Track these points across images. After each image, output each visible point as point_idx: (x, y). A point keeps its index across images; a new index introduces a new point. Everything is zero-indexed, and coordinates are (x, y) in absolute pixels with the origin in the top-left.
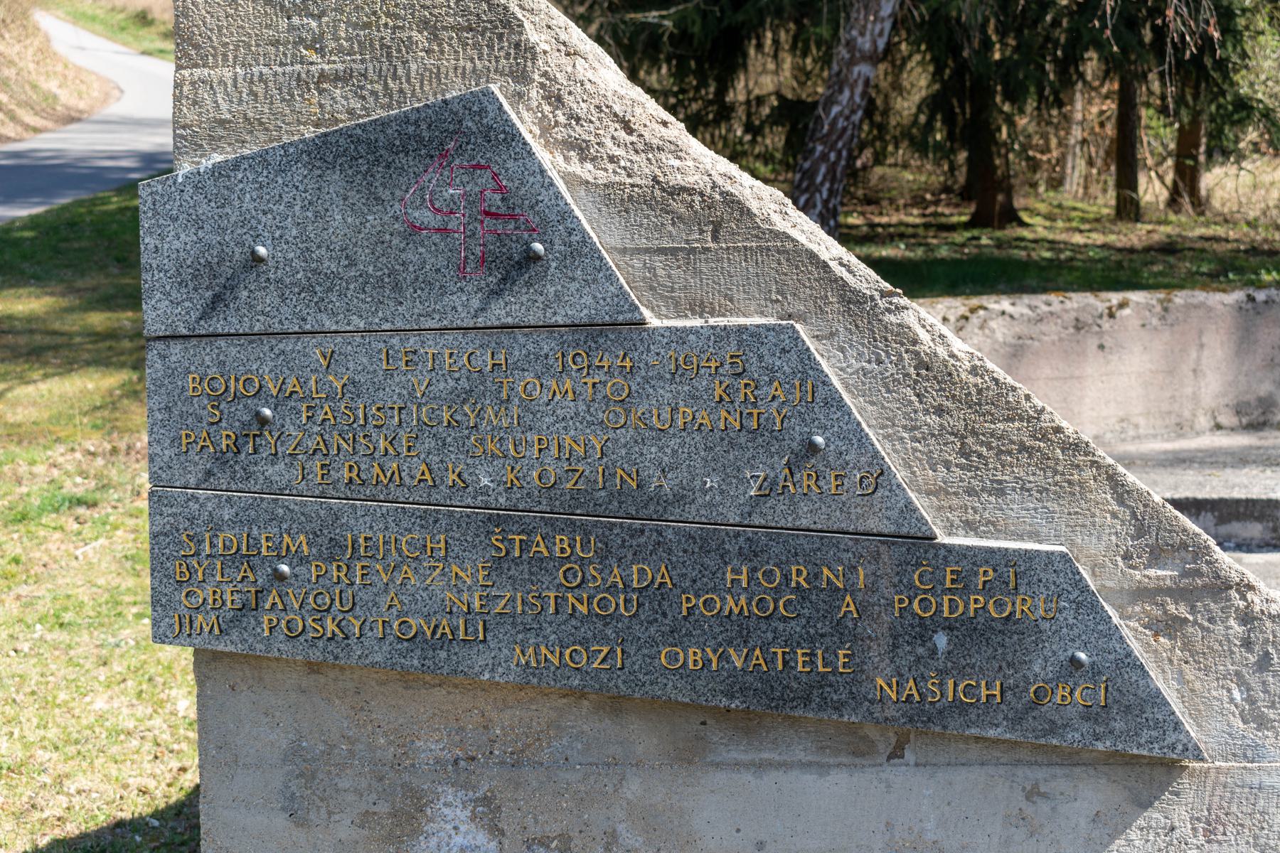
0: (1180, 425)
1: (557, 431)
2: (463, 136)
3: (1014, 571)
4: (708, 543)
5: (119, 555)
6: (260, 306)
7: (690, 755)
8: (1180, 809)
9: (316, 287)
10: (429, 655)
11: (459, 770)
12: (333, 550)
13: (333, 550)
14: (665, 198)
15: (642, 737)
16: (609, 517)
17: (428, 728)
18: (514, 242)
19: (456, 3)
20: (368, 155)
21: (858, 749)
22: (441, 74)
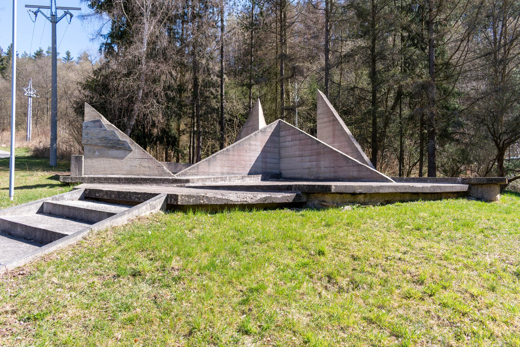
0: (55, 335)
1: (103, 134)
2: (99, 121)
3: (124, 141)
4: (110, 140)
5: (264, 62)
6: (88, 128)
7: (109, 150)
8: (132, 153)
9: (91, 127)
10: (96, 145)
11: (97, 150)
12: (92, 139)
13: (92, 139)
14: (108, 125)
15: (106, 149)
16: (105, 138)
17: (96, 148)
18: (101, 126)
19: (519, 93)
20: (94, 122)
21: (117, 149)
22: (98, 118)
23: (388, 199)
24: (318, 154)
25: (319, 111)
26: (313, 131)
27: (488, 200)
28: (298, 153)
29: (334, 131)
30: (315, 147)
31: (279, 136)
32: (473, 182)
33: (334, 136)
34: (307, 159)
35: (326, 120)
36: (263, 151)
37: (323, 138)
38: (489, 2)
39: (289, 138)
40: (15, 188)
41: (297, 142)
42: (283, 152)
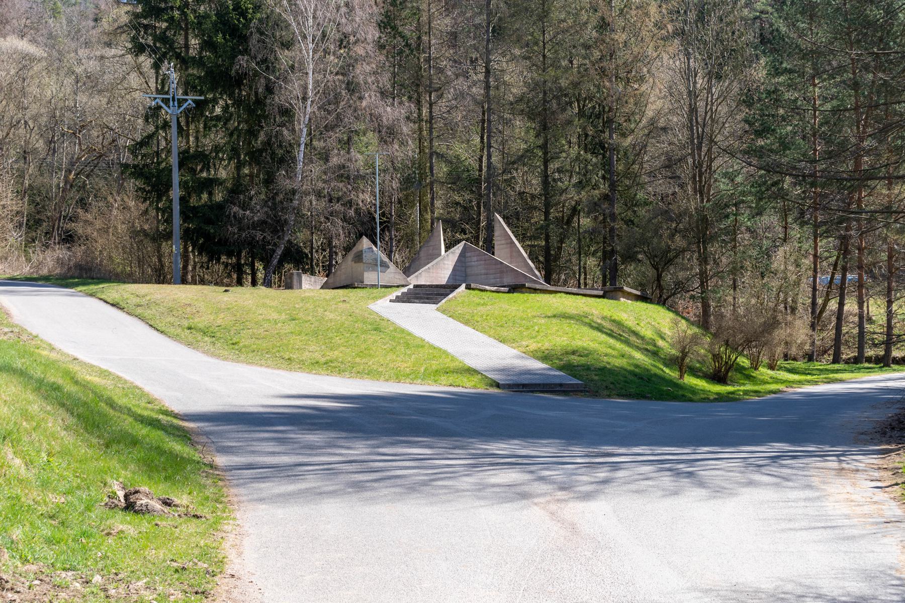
23: (574, 294)
24: (502, 272)
25: (497, 233)
26: (493, 254)
27: (616, 299)
28: (483, 271)
29: (511, 252)
30: (499, 266)
31: (465, 257)
32: (620, 293)
33: (511, 256)
34: (492, 276)
35: (503, 242)
36: (453, 270)
37: (501, 255)
38: (692, 26)
39: (475, 259)
40: (579, 287)
41: (482, 262)
42: (469, 271)
